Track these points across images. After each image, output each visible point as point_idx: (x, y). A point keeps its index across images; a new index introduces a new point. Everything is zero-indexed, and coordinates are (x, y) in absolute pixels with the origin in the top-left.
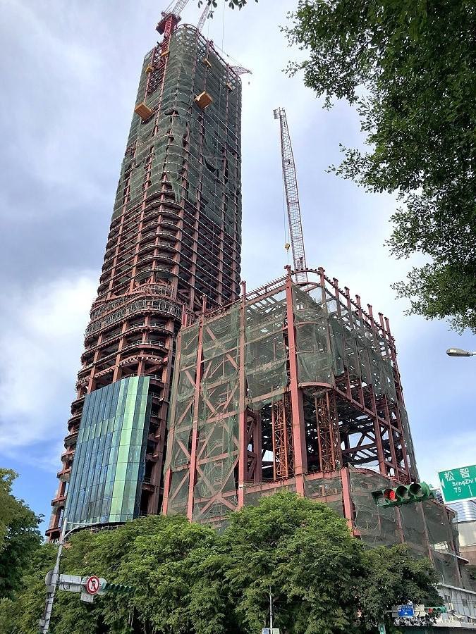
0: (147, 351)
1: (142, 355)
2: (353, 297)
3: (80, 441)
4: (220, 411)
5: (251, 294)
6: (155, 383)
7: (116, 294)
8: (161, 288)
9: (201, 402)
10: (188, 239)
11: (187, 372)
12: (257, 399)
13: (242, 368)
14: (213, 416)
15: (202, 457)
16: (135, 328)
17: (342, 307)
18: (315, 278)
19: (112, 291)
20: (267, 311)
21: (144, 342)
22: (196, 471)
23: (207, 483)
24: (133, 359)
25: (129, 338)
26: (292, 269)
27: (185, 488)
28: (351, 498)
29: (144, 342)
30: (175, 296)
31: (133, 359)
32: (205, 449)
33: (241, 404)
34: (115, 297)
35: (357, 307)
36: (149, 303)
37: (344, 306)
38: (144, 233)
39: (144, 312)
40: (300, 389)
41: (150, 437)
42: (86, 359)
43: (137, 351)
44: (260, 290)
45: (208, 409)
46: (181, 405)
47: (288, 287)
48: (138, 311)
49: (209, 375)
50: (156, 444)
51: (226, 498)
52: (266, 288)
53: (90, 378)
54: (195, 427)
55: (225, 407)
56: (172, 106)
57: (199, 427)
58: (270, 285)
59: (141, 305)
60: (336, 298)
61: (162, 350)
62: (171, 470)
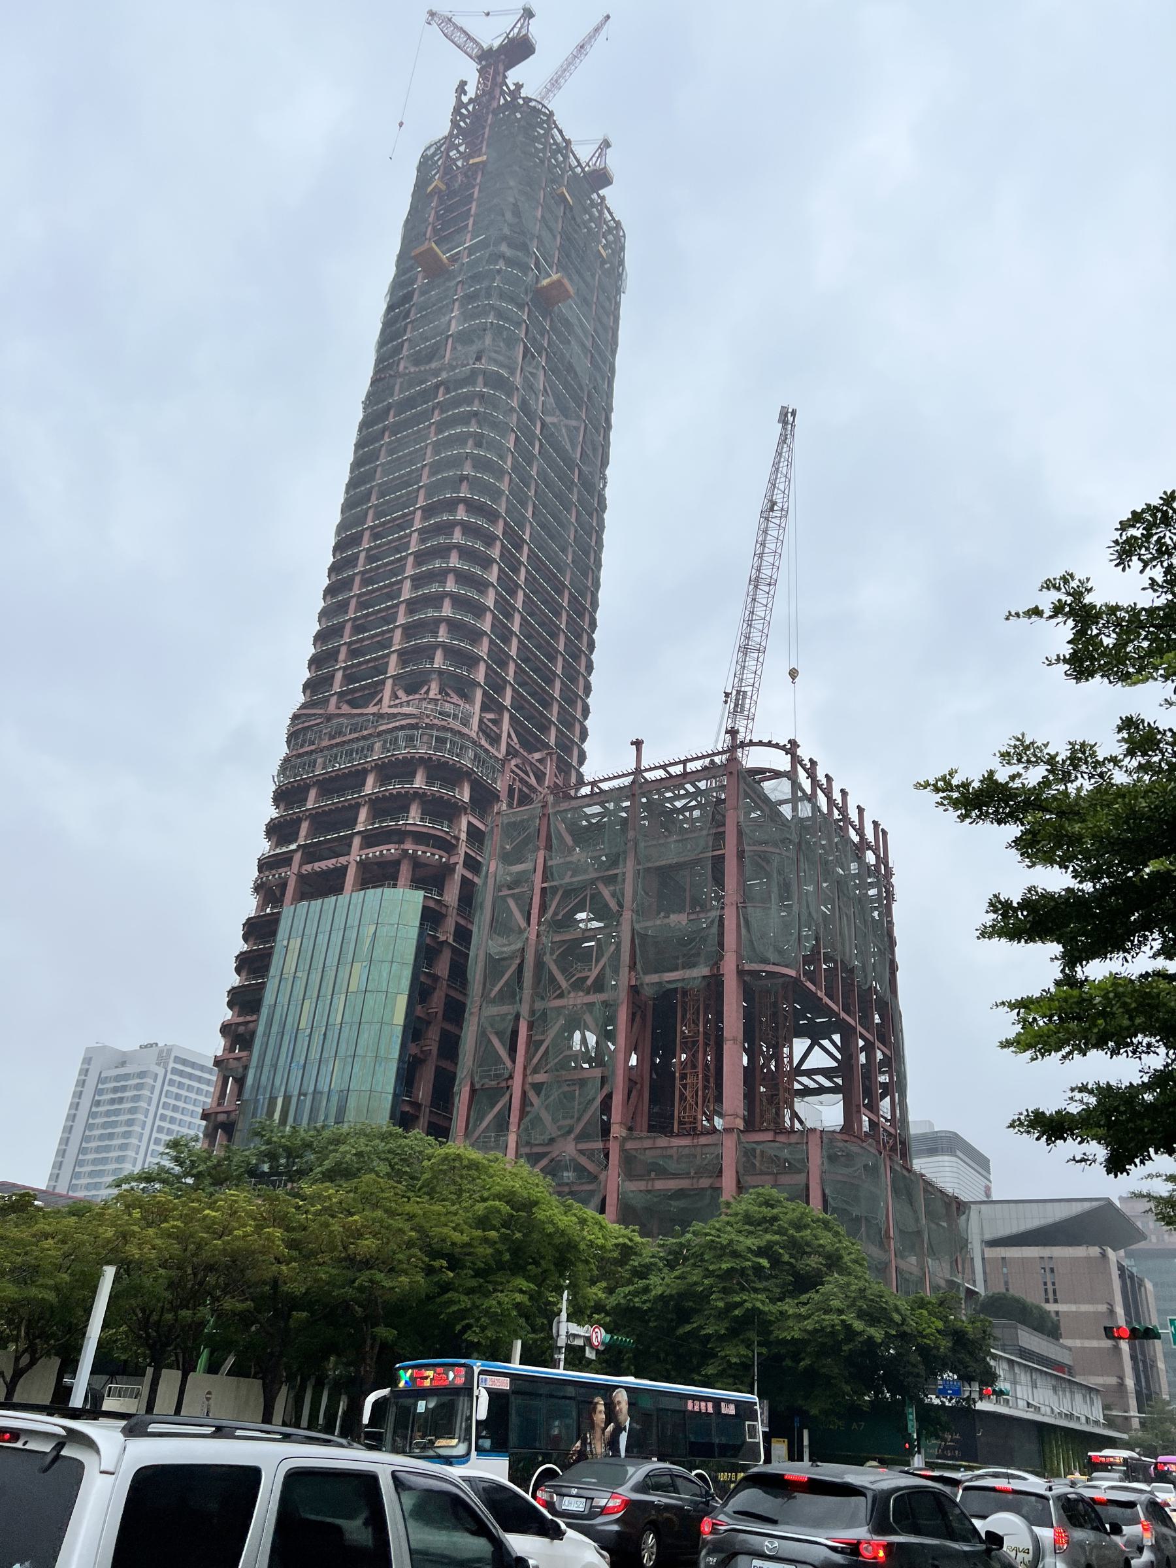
0: (420, 838)
1: (410, 847)
2: (837, 796)
3: (269, 997)
4: (578, 985)
5: (651, 769)
6: (432, 904)
7: (352, 704)
8: (448, 708)
9: (539, 965)
10: (505, 608)
11: (512, 903)
12: (654, 978)
13: (627, 915)
14: (561, 996)
15: (536, 1071)
16: (395, 787)
17: (800, 794)
18: (782, 762)
19: (341, 695)
20: (679, 804)
21: (414, 818)
22: (524, 1093)
23: (546, 1117)
24: (390, 850)
25: (383, 807)
26: (740, 737)
27: (502, 1124)
28: (823, 1182)
29: (414, 818)
30: (475, 727)
31: (390, 850)
32: (546, 1051)
33: (622, 981)
34: (346, 709)
35: (841, 813)
36: (425, 738)
37: (803, 791)
38: (418, 581)
39: (417, 756)
40: (740, 973)
41: (419, 1010)
42: (277, 831)
43: (399, 836)
44: (671, 764)
45: (552, 979)
46: (495, 966)
47: (731, 773)
48: (403, 752)
49: (556, 913)
50: (429, 1023)
51: (581, 1152)
52: (685, 762)
53: (291, 873)
54: (525, 1010)
55: (589, 982)
56: (488, 296)
57: (532, 1012)
58: (693, 759)
59: (410, 739)
60: (791, 776)
61: (449, 838)
62: (472, 1084)
